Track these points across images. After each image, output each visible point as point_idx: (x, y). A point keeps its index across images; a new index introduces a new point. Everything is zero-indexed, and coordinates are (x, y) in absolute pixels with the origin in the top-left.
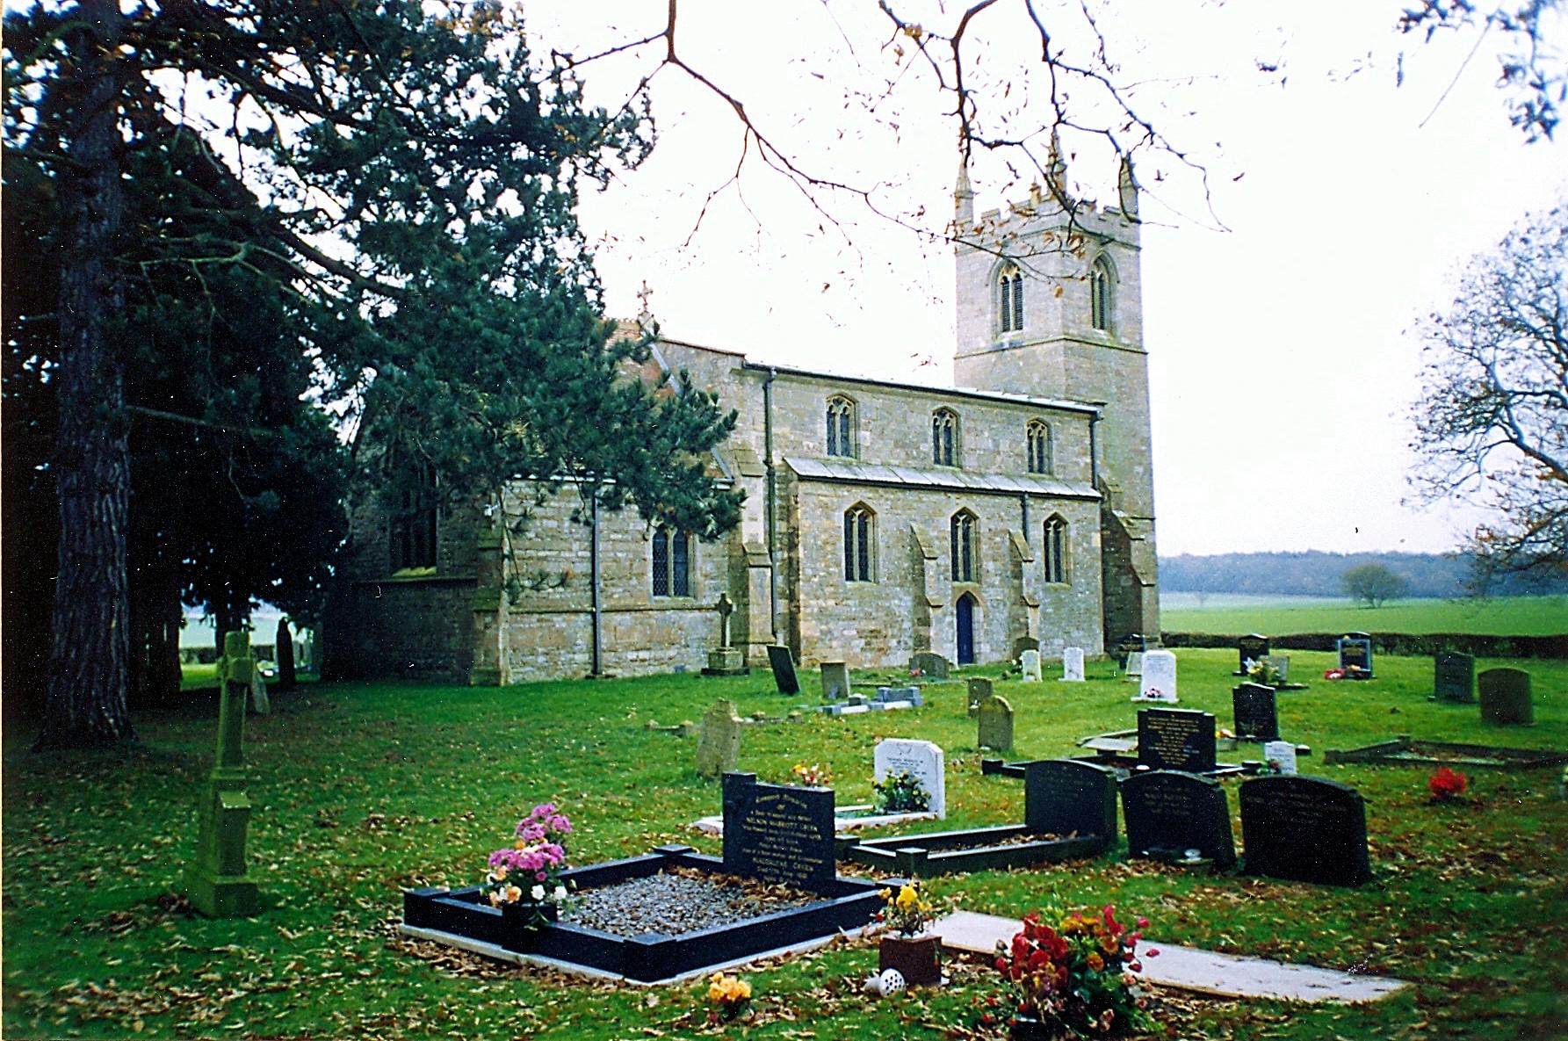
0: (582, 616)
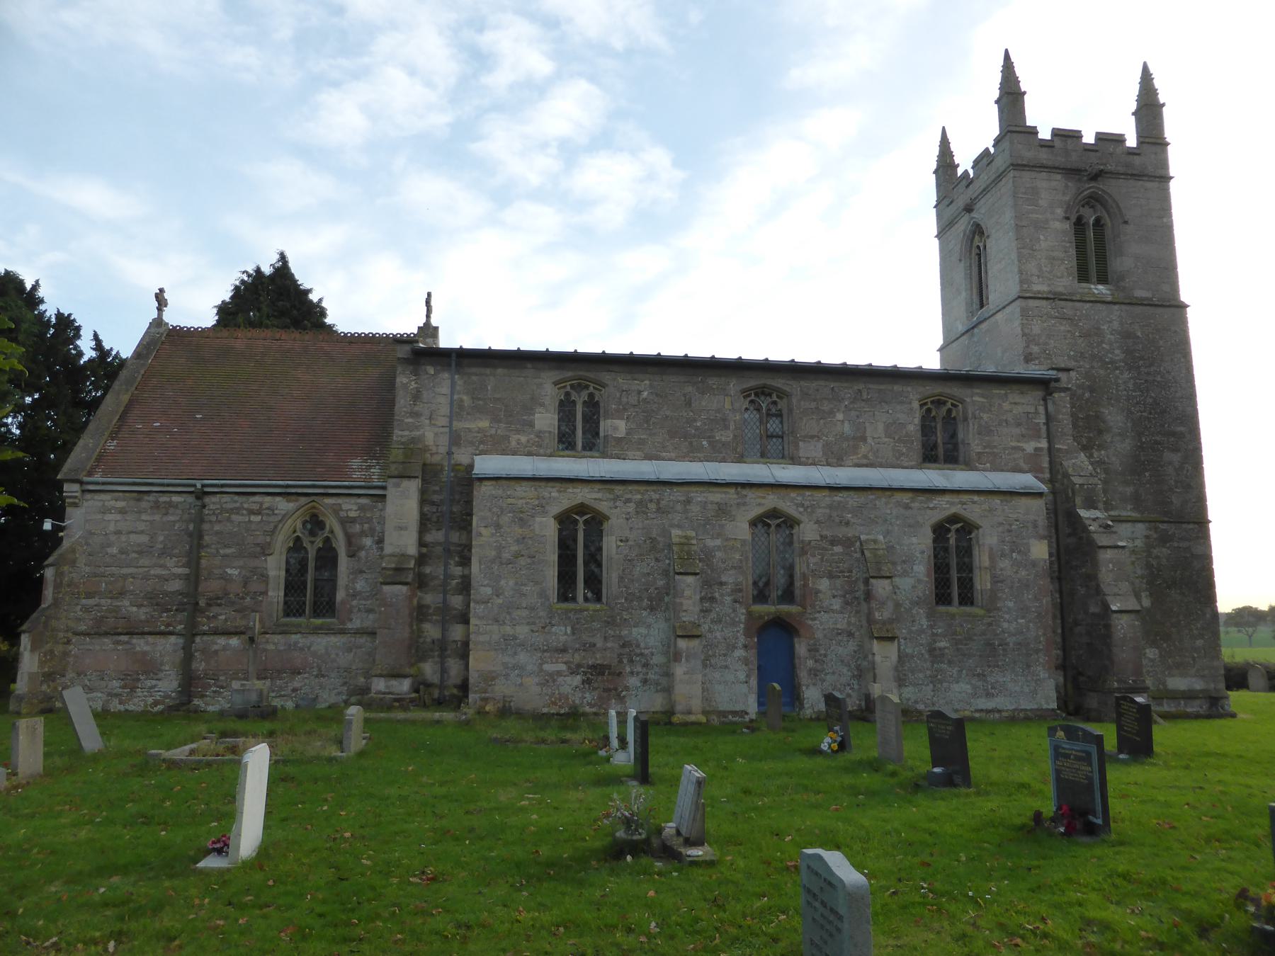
0: (173, 639)
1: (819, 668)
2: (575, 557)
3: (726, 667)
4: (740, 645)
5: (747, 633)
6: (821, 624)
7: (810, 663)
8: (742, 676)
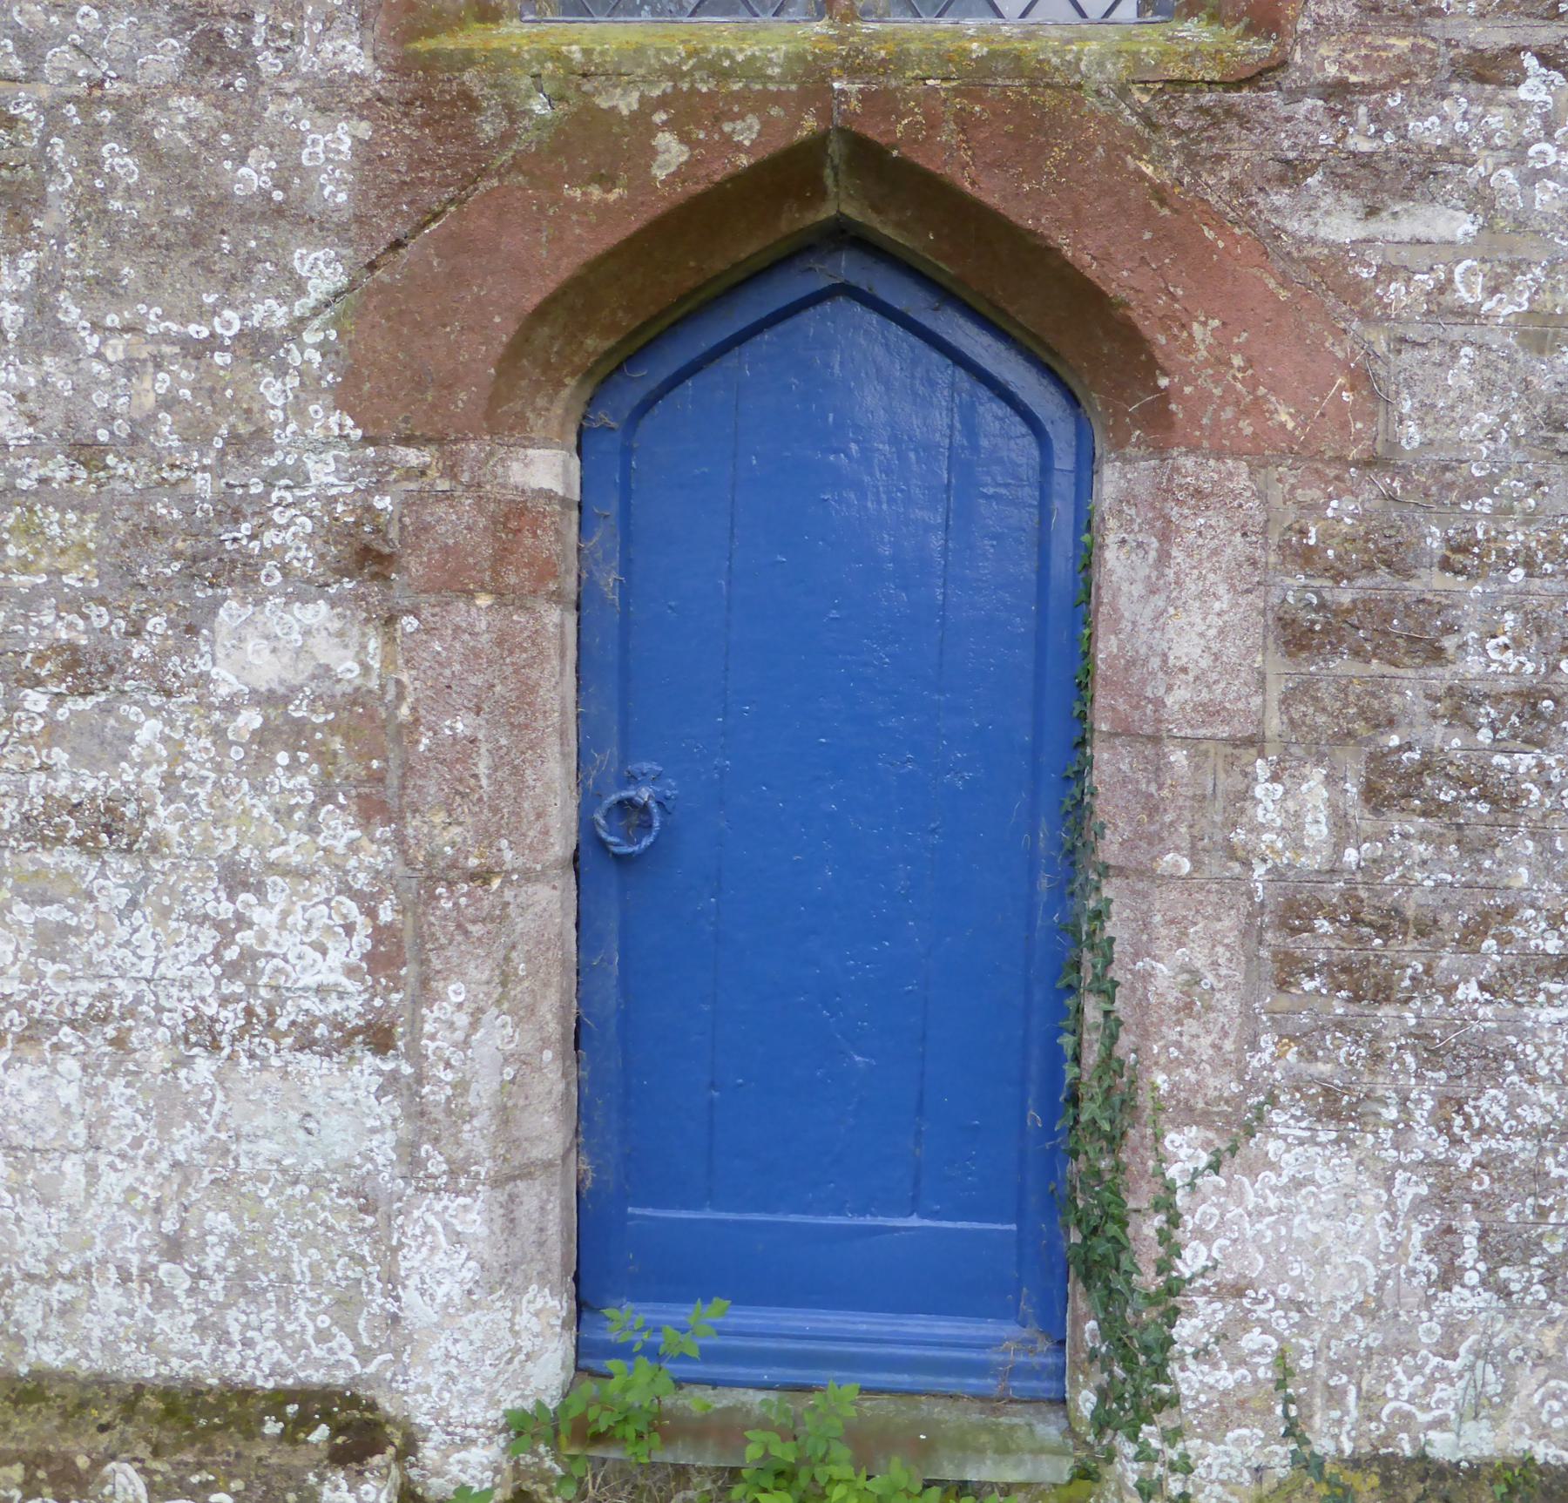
1: (1421, 866)
2: (805, 1212)
3: (107, 826)
4: (292, 535)
5: (390, 389)
6: (1506, 240)
7: (1297, 815)
8: (315, 955)
